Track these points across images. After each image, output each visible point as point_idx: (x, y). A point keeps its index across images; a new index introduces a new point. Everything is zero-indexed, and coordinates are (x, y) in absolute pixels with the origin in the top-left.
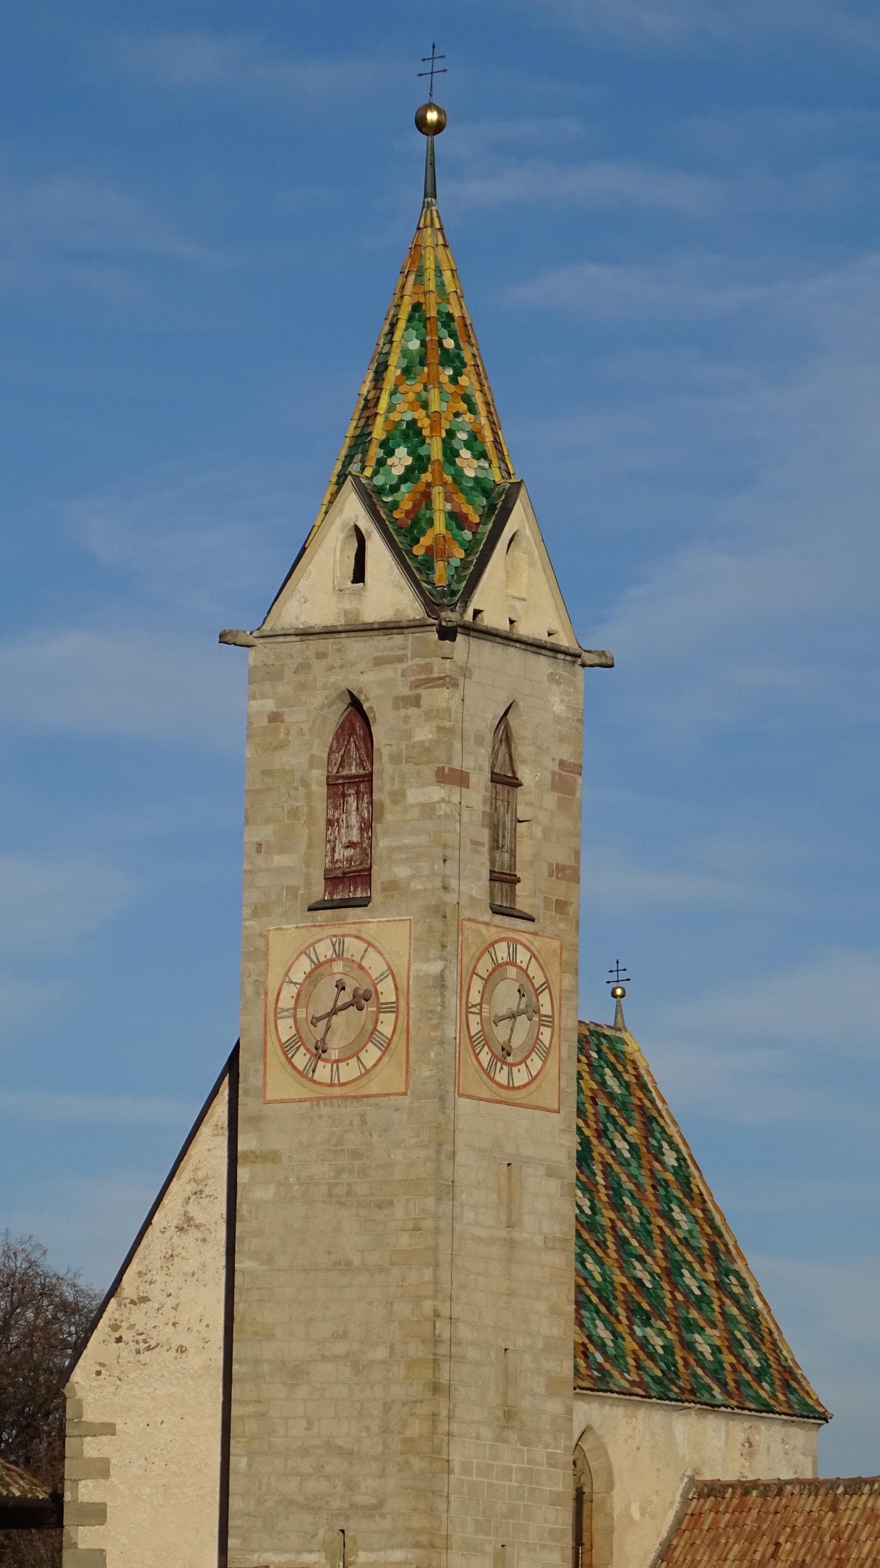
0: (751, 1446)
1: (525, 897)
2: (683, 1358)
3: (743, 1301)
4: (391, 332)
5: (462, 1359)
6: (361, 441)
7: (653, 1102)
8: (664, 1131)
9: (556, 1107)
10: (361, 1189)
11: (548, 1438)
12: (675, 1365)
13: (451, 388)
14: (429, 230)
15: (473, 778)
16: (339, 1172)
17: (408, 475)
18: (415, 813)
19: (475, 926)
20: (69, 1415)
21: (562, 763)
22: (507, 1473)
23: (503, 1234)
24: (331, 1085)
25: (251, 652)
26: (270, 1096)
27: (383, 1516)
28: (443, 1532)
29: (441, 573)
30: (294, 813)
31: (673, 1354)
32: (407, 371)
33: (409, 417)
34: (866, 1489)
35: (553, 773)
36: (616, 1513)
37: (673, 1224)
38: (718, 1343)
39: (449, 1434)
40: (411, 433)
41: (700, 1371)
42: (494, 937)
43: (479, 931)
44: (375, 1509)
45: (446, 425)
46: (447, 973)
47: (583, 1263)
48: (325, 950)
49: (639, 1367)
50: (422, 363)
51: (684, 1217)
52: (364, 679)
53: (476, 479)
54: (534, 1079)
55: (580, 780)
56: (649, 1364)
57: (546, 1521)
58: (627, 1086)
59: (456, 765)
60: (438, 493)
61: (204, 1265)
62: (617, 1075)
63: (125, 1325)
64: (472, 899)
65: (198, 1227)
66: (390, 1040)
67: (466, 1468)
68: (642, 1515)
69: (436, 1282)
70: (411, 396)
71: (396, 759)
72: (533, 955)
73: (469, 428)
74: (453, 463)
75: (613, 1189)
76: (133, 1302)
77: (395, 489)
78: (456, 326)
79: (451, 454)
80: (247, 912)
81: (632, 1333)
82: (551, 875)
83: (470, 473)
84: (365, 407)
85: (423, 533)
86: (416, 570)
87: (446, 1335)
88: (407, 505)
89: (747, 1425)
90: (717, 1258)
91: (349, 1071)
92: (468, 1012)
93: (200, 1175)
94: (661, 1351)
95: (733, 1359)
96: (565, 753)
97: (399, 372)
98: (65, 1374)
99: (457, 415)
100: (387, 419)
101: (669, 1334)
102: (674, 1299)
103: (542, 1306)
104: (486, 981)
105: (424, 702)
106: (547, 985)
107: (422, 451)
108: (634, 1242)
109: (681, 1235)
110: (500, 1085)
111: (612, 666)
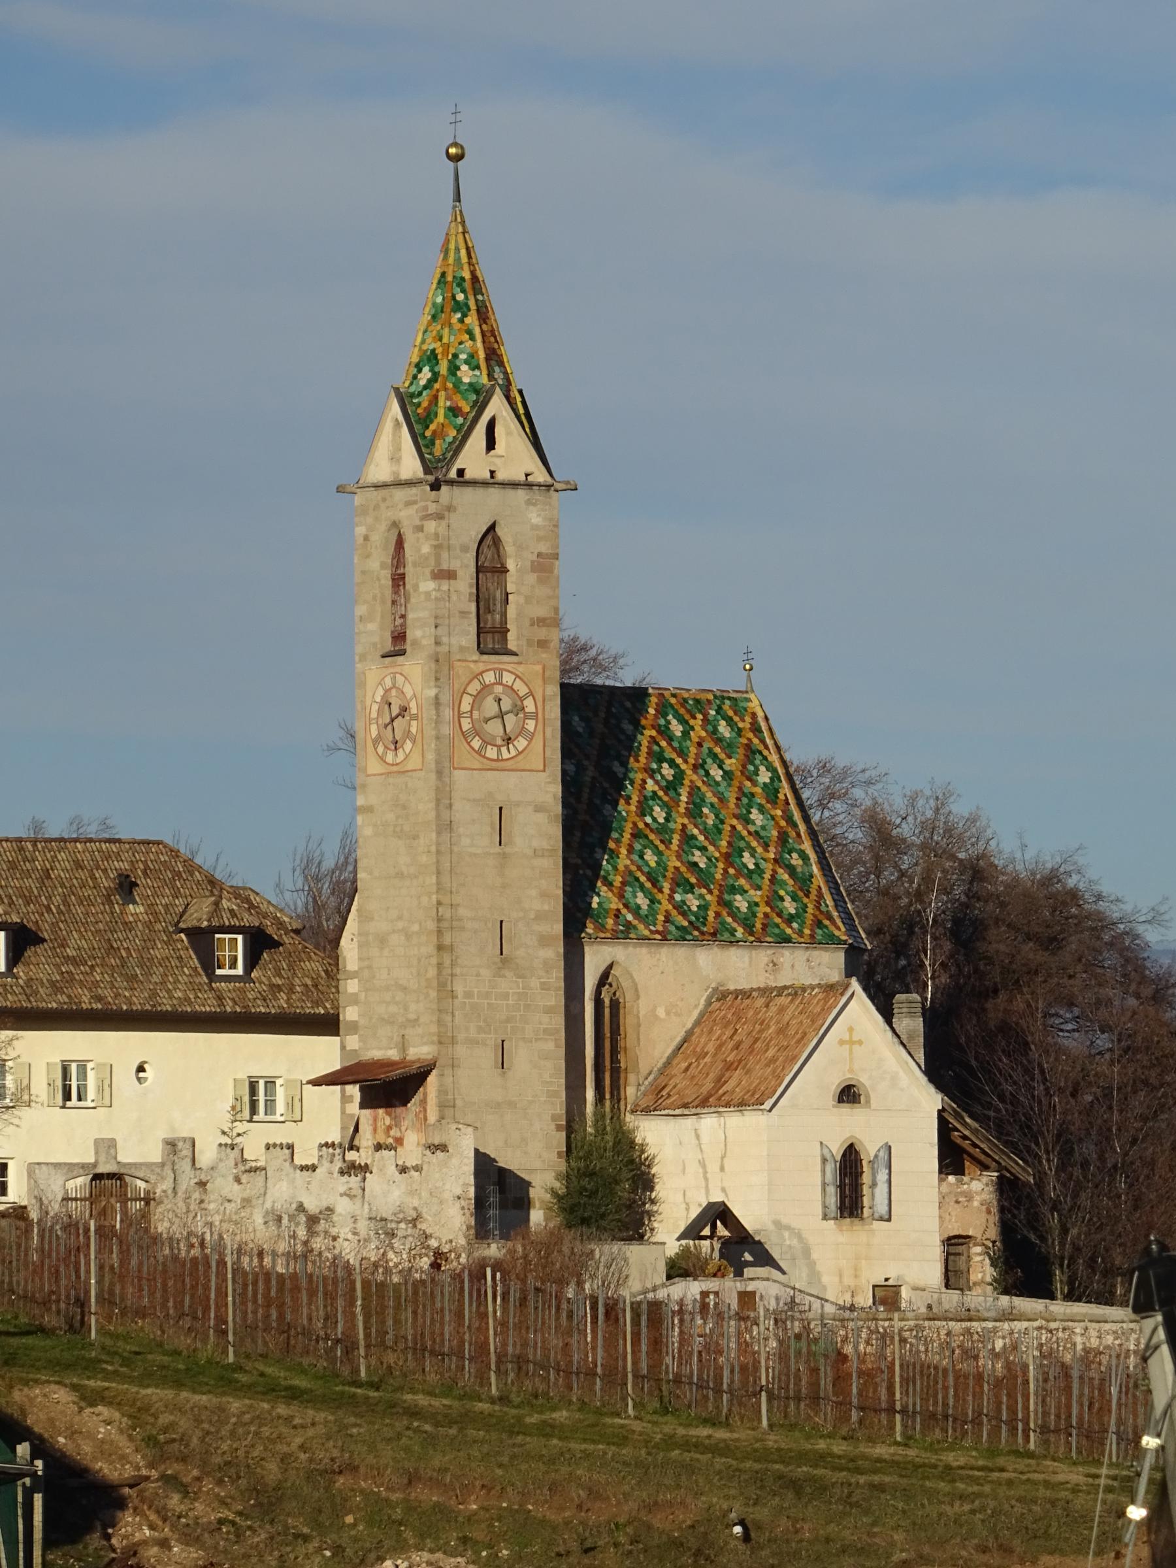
0: (775, 965)
5: (463, 929)
10: (406, 828)
11: (542, 973)
15: (460, 573)
16: (398, 817)
18: (423, 597)
19: (464, 664)
21: (539, 555)
22: (506, 996)
23: (498, 849)
26: (370, 772)
28: (450, 1034)
29: (439, 448)
30: (374, 598)
33: (431, 347)
35: (533, 562)
36: (641, 1014)
39: (452, 975)
43: (469, 667)
44: (415, 1022)
45: (452, 350)
50: (442, 311)
53: (470, 384)
55: (557, 563)
57: (540, 1023)
59: (445, 567)
60: (442, 395)
64: (462, 649)
67: (468, 995)
68: (668, 1013)
69: (438, 883)
70: (434, 333)
71: (415, 565)
73: (469, 350)
74: (454, 375)
75: (694, 803)
79: (454, 369)
80: (357, 658)
81: (671, 898)
82: (532, 625)
83: (466, 380)
85: (432, 422)
86: (422, 444)
87: (448, 915)
88: (425, 404)
89: (769, 952)
96: (544, 548)
100: (420, 349)
103: (533, 892)
106: (531, 693)
107: (436, 369)
109: (752, 828)
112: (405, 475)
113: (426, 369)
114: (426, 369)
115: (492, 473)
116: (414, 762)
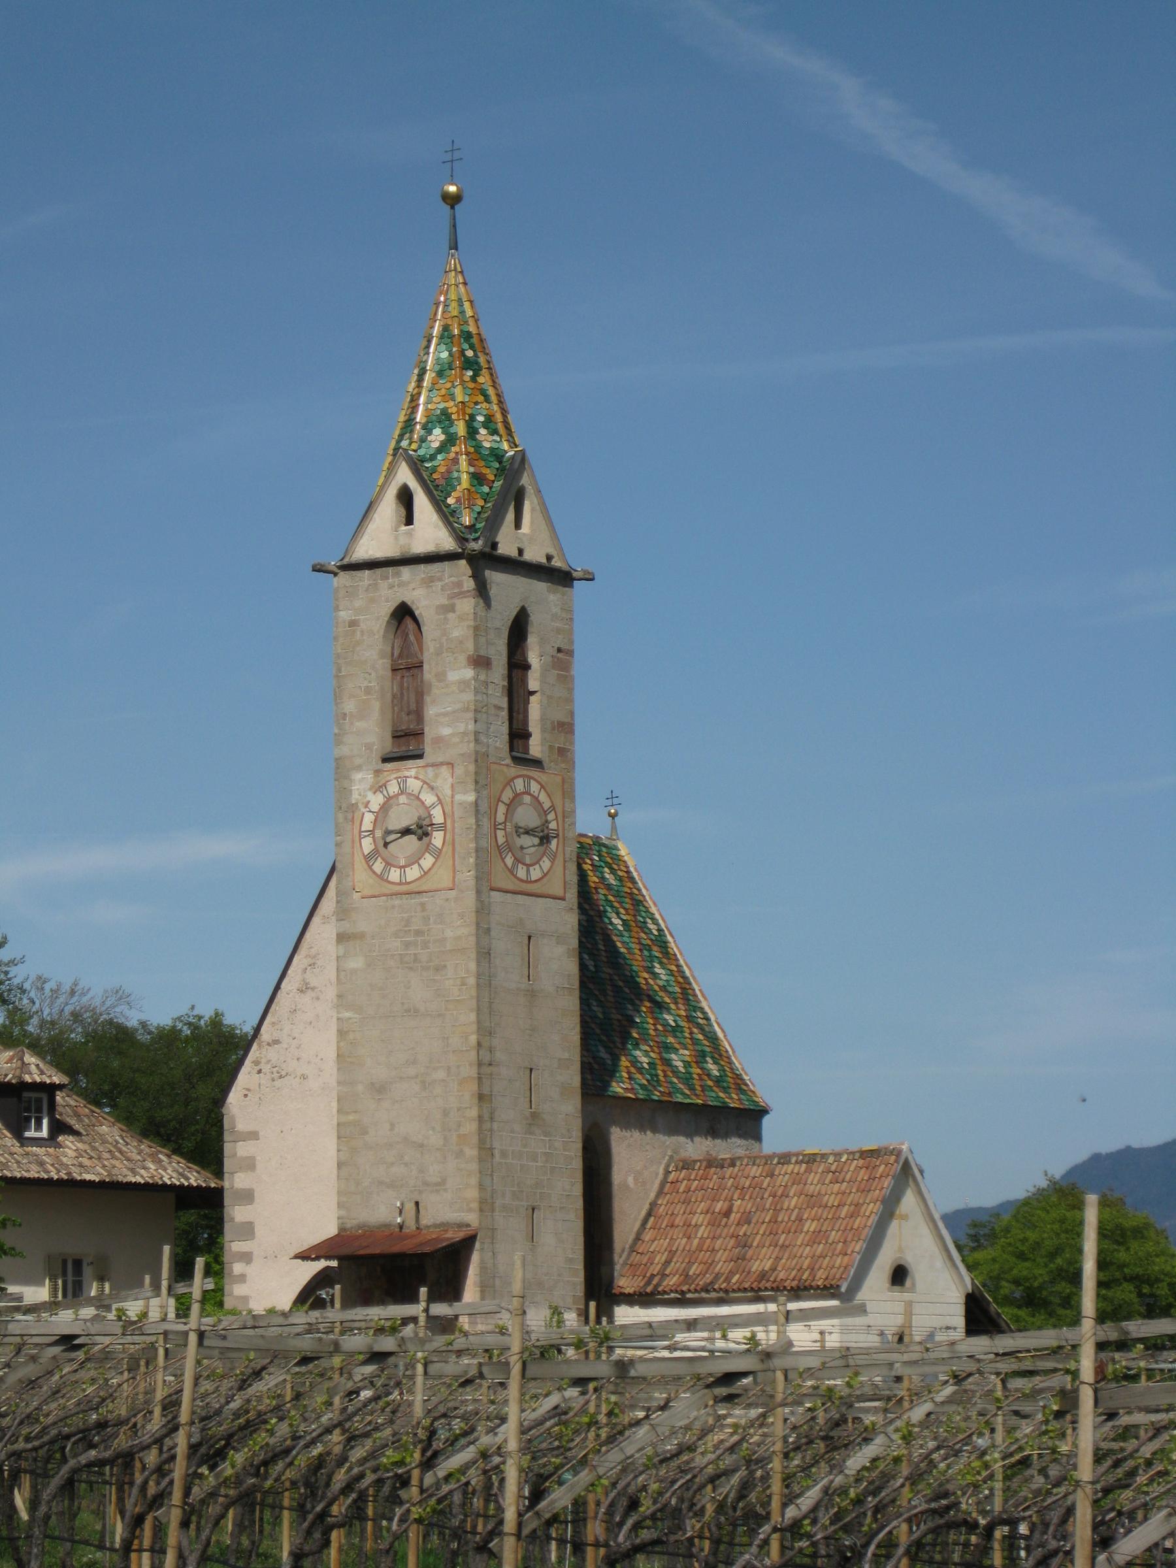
1: (536, 747)
2: (664, 1071)
3: (707, 1029)
4: (428, 347)
6: (409, 423)
7: (639, 890)
8: (647, 911)
9: (560, 893)
12: (657, 1075)
13: (472, 385)
14: (453, 273)
15: (494, 663)
16: (407, 945)
17: (442, 448)
20: (226, 1126)
24: (400, 884)
25: (336, 579)
27: (446, 1190)
31: (655, 1069)
32: (440, 374)
34: (794, 1160)
37: (655, 976)
38: (689, 1059)
40: (444, 419)
41: (675, 1080)
42: (513, 775)
46: (480, 802)
47: (589, 1005)
48: (393, 788)
49: (630, 1078)
51: (663, 972)
52: (415, 593)
53: (491, 449)
54: (545, 875)
56: (638, 1076)
58: (620, 879)
61: (318, 1016)
62: (613, 871)
63: (263, 1061)
65: (313, 989)
66: (441, 850)
67: (504, 1154)
72: (542, 787)
76: (269, 1044)
77: (433, 458)
78: (475, 340)
79: (472, 432)
82: (553, 729)
83: (487, 445)
84: (412, 401)
90: (687, 1000)
91: (413, 873)
92: (496, 829)
93: (313, 951)
94: (646, 1066)
95: (699, 1071)
97: (434, 375)
98: (219, 1101)
99: (476, 403)
101: (652, 1054)
102: (656, 1030)
104: (508, 805)
105: (458, 607)
107: (452, 430)
108: (627, 990)
109: (661, 983)
110: (522, 880)
111: (592, 579)
112: (420, 546)
113: (437, 431)
114: (437, 431)
115: (521, 552)
116: (443, 877)
